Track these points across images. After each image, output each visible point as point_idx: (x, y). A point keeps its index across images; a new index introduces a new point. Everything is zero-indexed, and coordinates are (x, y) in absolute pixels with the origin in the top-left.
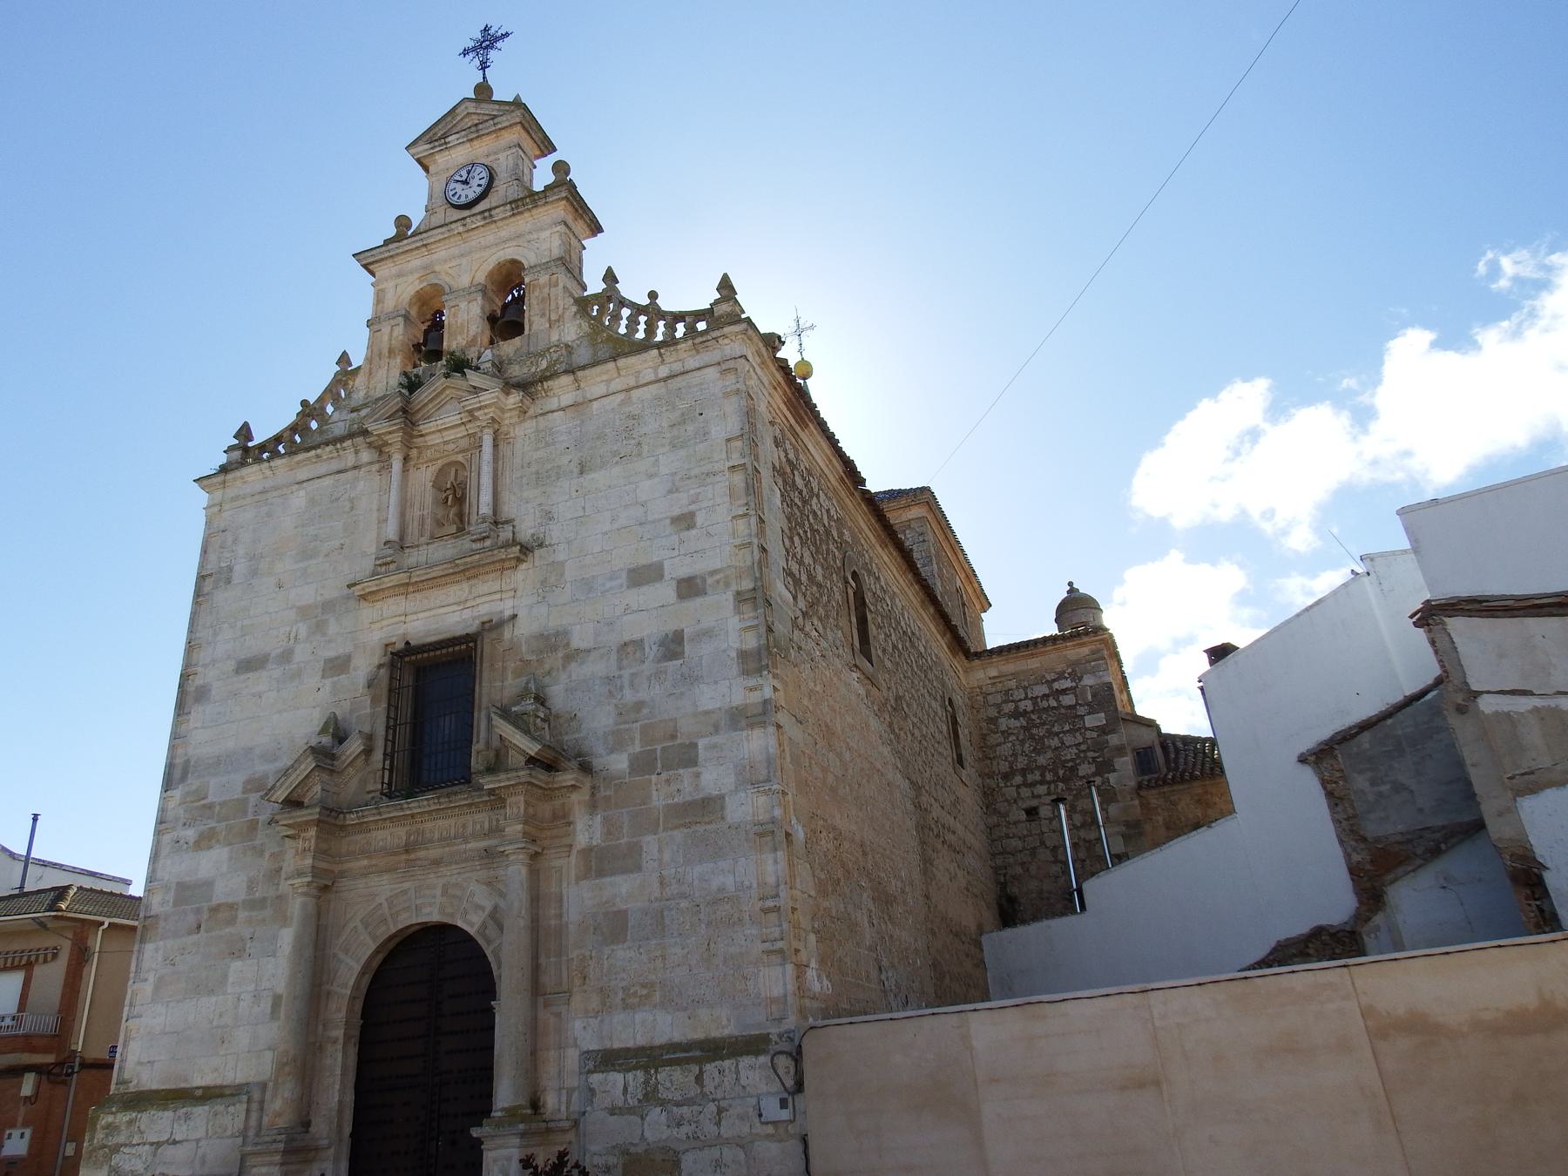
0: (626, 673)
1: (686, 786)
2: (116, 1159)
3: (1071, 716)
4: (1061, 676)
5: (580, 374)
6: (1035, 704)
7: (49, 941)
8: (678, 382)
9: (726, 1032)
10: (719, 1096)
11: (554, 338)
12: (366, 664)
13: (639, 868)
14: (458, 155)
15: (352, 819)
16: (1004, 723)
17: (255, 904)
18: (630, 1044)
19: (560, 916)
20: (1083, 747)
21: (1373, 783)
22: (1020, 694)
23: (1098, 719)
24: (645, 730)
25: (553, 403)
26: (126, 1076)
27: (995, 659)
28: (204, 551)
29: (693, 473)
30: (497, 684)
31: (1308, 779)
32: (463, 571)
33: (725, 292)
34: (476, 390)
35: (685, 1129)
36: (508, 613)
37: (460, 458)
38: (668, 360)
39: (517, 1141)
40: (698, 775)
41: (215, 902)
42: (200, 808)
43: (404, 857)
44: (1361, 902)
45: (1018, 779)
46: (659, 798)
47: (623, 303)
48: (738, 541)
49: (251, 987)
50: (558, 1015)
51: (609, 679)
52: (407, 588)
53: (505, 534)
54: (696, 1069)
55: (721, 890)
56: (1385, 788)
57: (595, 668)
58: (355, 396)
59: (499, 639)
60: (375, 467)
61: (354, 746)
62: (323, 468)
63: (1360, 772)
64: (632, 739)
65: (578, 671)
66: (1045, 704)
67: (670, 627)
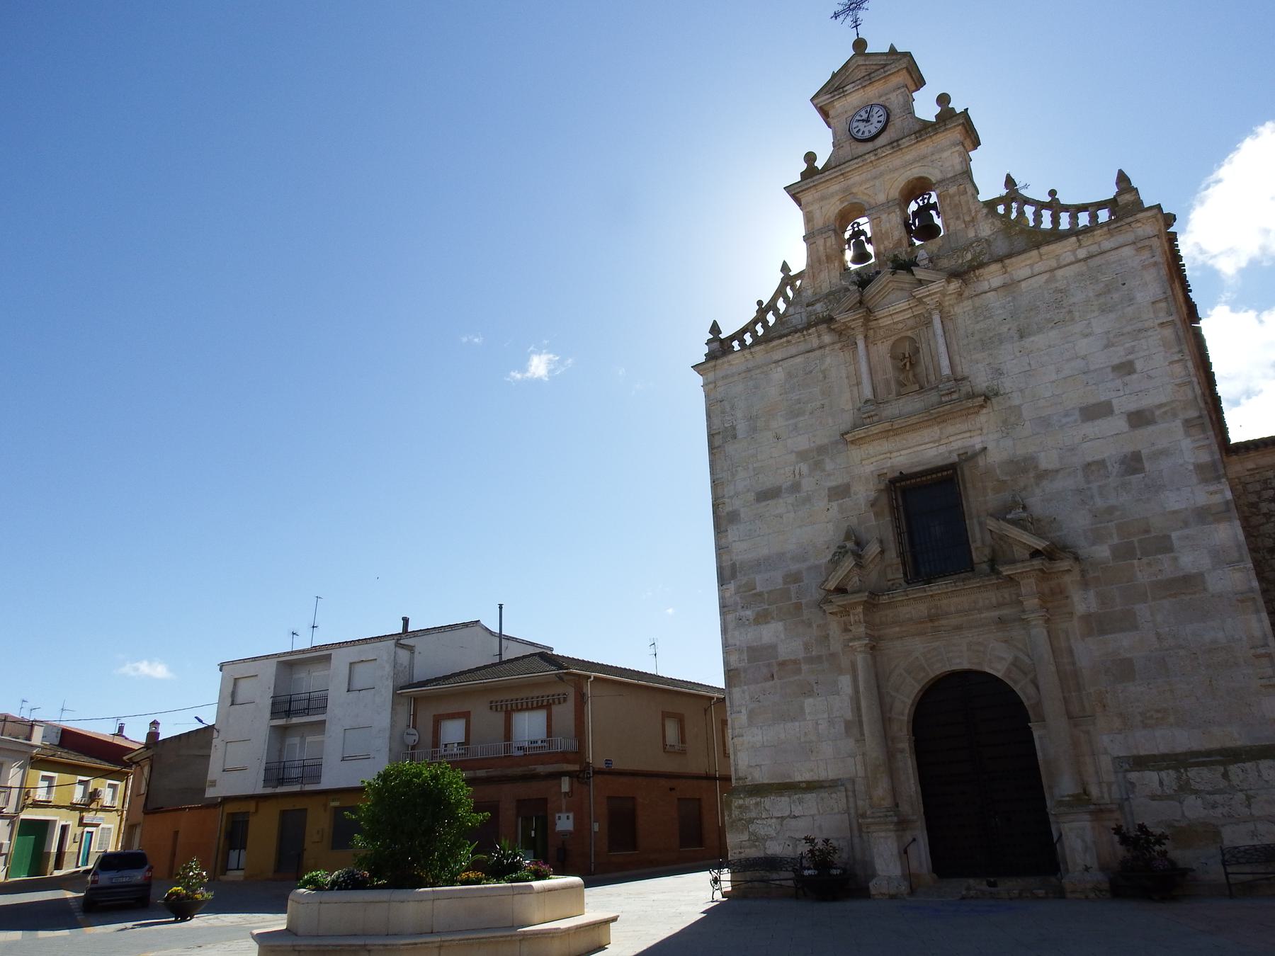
2: (752, 828)
5: (1007, 262)
7: (560, 689)
8: (1094, 262)
9: (1239, 743)
11: (971, 234)
12: (864, 492)
14: (854, 99)
15: (884, 599)
18: (1156, 752)
19: (1074, 664)
25: (985, 286)
27: (1252, 454)
29: (1125, 330)
30: (980, 501)
32: (935, 416)
33: (1123, 185)
34: (921, 282)
36: (978, 447)
37: (909, 334)
38: (1084, 243)
39: (1087, 817)
40: (1176, 559)
41: (780, 659)
43: (930, 624)
47: (1027, 201)
49: (826, 716)
50: (1088, 732)
51: (1080, 491)
52: (886, 434)
53: (965, 388)
60: (838, 346)
61: (873, 549)
62: (793, 350)
67: (1129, 449)
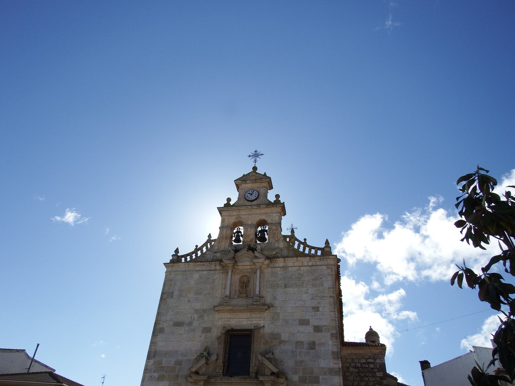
4: (370, 358)
5: (286, 259)
6: (361, 365)
8: (315, 268)
11: (277, 245)
12: (216, 332)
14: (249, 185)
16: (351, 369)
20: (375, 382)
22: (357, 361)
29: (319, 295)
30: (258, 347)
32: (250, 309)
36: (262, 325)
37: (248, 274)
52: (231, 311)
53: (262, 301)
60: (221, 272)
62: (204, 268)
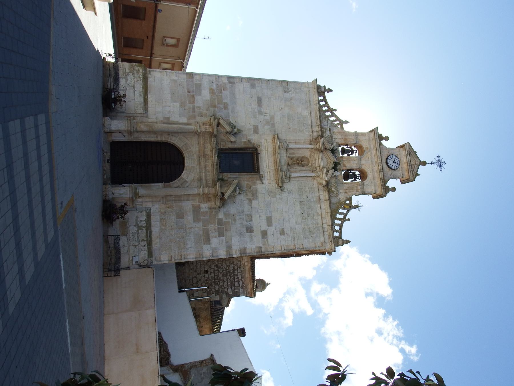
0: (244, 217)
1: (213, 234)
2: (131, 74)
3: (232, 285)
4: (243, 283)
9: (153, 246)
10: (139, 246)
11: (341, 191)
12: (255, 139)
13: (194, 222)
14: (404, 158)
16: (232, 266)
17: (194, 108)
18: (152, 221)
19: (184, 200)
21: (204, 373)
22: (239, 271)
23: (230, 293)
24: (229, 222)
26: (152, 73)
28: (295, 82)
30: (245, 179)
31: (207, 356)
32: (278, 168)
35: (132, 237)
36: (264, 182)
37: (310, 164)
39: (131, 196)
40: (216, 237)
41: (195, 96)
42: (221, 88)
44: (175, 366)
45: (216, 269)
46: (211, 227)
47: (348, 211)
48: (275, 248)
50: (160, 201)
51: (243, 212)
53: (286, 180)
54: (145, 239)
55: (187, 244)
56: (203, 375)
57: (246, 208)
58: (334, 128)
59: (257, 180)
60: (311, 138)
61: (233, 139)
63: (207, 370)
64: (227, 219)
65: (246, 202)
66: (236, 278)
67: (255, 229)
